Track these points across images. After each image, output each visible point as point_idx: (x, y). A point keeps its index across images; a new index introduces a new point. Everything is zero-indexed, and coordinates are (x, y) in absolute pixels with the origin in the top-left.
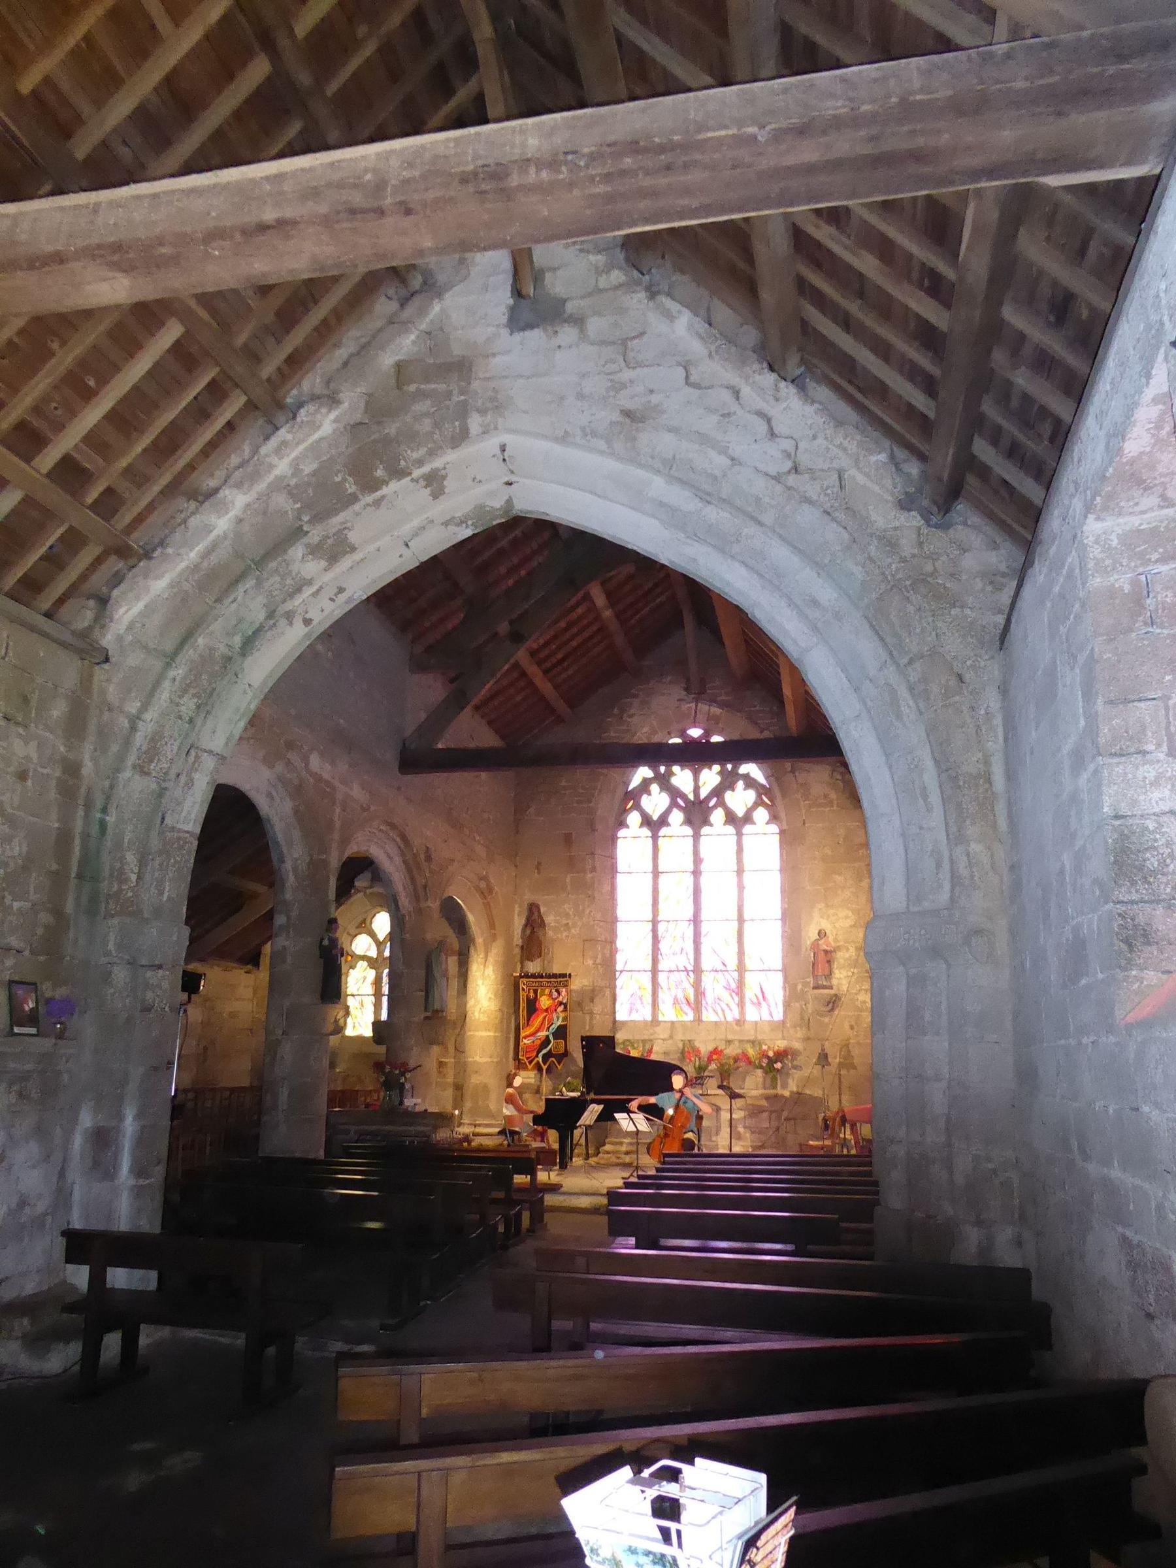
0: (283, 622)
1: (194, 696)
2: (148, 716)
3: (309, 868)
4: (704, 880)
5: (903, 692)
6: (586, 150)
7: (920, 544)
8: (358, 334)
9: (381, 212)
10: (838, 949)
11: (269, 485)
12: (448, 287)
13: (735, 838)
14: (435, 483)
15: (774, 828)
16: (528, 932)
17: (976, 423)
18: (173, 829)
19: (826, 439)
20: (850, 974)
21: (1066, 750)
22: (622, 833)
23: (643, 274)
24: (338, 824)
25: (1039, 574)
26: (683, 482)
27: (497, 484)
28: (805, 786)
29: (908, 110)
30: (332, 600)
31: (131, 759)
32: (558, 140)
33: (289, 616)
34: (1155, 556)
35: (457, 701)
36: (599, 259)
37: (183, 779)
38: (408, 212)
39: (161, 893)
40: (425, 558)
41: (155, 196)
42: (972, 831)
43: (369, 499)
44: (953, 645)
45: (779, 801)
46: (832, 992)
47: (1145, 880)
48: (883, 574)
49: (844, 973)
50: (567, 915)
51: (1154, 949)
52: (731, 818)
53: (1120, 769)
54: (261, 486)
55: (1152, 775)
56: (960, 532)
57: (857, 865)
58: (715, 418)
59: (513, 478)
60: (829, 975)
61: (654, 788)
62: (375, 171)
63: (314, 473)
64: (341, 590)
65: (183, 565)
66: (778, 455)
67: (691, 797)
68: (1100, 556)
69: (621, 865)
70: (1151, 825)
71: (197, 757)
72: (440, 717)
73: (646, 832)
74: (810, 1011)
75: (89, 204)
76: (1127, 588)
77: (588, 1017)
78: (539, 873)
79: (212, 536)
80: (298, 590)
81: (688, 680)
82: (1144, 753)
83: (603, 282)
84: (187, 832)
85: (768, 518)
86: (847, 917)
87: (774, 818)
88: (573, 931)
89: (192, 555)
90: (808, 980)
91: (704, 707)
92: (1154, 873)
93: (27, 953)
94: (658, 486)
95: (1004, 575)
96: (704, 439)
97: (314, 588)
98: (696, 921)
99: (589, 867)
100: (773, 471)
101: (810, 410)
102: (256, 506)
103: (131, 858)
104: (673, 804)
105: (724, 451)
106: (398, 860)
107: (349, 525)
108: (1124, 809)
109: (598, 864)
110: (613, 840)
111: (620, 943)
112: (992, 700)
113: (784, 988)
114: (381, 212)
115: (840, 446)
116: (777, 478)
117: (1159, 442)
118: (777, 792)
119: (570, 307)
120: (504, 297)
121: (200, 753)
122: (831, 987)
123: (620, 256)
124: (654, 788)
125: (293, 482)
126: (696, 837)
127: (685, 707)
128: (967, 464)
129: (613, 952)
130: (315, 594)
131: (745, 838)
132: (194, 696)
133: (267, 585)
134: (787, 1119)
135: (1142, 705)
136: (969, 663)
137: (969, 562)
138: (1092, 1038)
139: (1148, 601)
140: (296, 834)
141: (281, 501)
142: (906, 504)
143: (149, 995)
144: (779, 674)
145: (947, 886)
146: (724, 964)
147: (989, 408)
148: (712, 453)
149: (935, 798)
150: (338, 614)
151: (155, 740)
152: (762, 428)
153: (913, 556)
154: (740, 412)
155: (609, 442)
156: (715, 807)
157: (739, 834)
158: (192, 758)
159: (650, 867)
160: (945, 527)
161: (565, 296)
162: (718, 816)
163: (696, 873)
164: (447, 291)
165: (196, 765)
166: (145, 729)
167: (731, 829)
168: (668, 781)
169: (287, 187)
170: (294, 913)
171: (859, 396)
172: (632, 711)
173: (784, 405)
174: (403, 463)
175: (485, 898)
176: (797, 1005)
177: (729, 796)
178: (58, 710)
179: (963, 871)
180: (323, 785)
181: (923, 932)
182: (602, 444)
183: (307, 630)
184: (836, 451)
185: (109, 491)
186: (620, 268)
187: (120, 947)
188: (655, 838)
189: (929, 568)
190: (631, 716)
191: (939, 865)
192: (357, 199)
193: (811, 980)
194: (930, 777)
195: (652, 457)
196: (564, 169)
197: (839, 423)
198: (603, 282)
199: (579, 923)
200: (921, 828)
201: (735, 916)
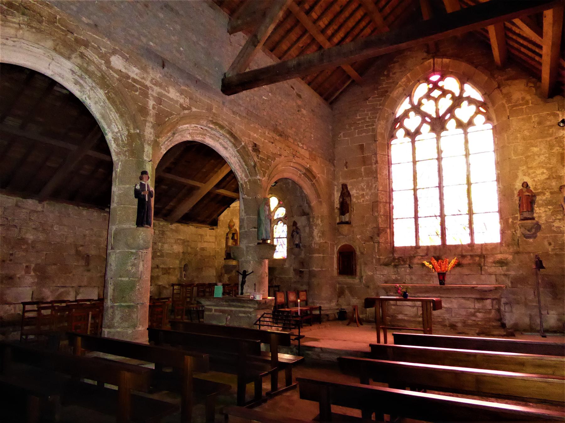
3: (128, 139)
4: (443, 163)
10: (539, 194)
13: (463, 135)
15: (489, 126)
16: (341, 200)
22: (393, 142)
24: (152, 112)
28: (508, 97)
35: (253, 42)
45: (491, 110)
49: (543, 209)
50: (363, 190)
52: (460, 124)
57: (548, 139)
60: (532, 210)
61: (412, 114)
67: (434, 115)
69: (394, 160)
73: (408, 139)
74: (519, 235)
77: (376, 245)
78: (347, 168)
86: (543, 173)
87: (489, 119)
88: (366, 197)
90: (516, 215)
98: (440, 187)
104: (424, 121)
109: (379, 159)
110: (389, 146)
111: (395, 203)
113: (500, 222)
118: (490, 105)
122: (533, 219)
124: (412, 114)
126: (438, 138)
127: (426, 63)
129: (391, 209)
131: (469, 135)
134: (506, 304)
146: (459, 211)
156: (450, 118)
157: (466, 133)
162: (451, 124)
163: (439, 159)
167: (461, 131)
168: (419, 109)
172: (395, 71)
175: (312, 181)
176: (509, 232)
180: (130, 81)
188: (413, 142)
190: (394, 73)
193: (518, 215)
199: (370, 193)
201: (465, 182)
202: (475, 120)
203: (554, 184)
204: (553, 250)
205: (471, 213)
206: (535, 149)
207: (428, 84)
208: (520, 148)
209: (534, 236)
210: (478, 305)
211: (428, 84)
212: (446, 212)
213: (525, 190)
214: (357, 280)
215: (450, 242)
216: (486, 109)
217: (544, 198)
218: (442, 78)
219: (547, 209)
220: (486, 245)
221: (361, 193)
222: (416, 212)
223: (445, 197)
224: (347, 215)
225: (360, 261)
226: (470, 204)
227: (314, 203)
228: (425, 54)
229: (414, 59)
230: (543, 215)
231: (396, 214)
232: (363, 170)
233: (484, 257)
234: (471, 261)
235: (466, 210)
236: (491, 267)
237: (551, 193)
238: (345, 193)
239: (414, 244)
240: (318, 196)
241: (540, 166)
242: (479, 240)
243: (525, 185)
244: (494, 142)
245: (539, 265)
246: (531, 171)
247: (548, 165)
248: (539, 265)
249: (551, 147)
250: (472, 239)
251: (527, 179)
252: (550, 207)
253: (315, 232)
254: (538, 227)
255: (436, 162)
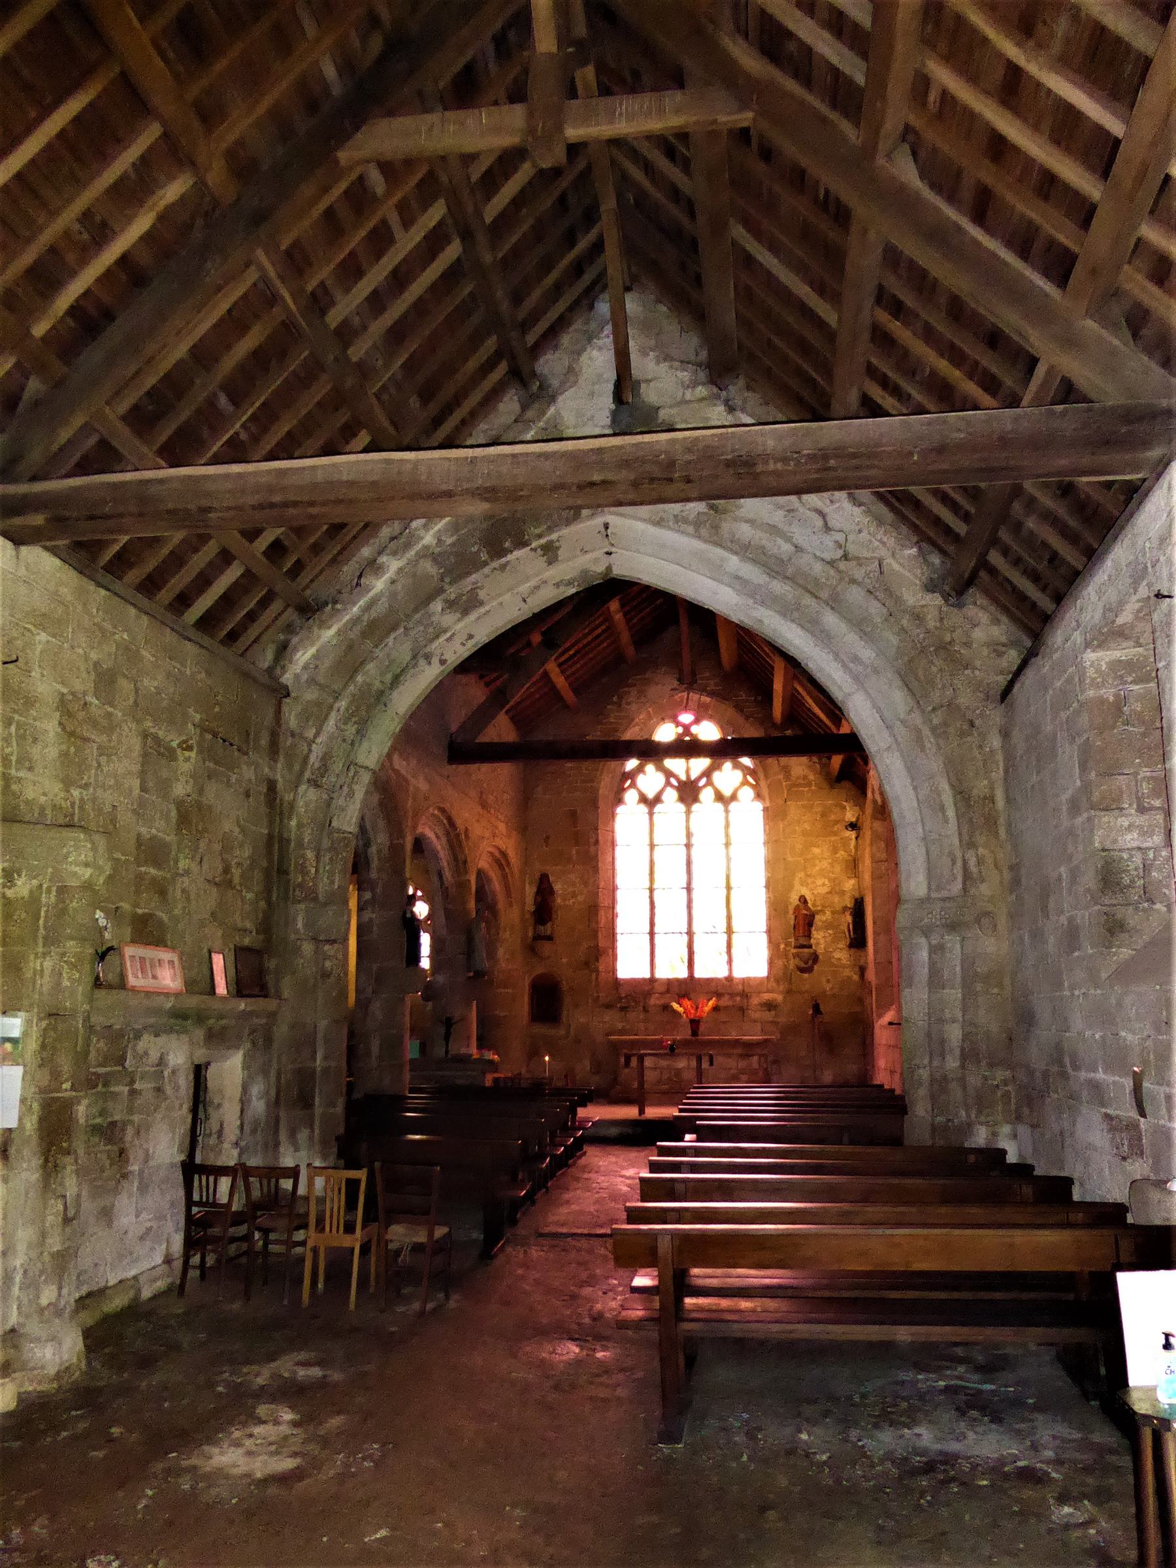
0: (422, 662)
1: (355, 723)
2: (319, 740)
4: (694, 851)
5: (926, 732)
6: (805, 452)
7: (942, 619)
8: (486, 427)
9: (671, 480)
10: (818, 912)
11: (417, 553)
12: (562, 389)
14: (550, 552)
17: (994, 541)
18: (339, 831)
19: (870, 534)
20: (827, 935)
21: (1065, 797)
23: (721, 390)
25: (1042, 666)
26: (754, 561)
27: (599, 553)
29: (1004, 441)
30: (463, 645)
31: (307, 775)
32: (787, 443)
33: (428, 658)
34: (1130, 679)
35: (498, 699)
36: (685, 376)
37: (345, 789)
38: (689, 481)
39: (333, 882)
40: (536, 610)
41: (514, 456)
42: (980, 839)
43: (496, 564)
44: (965, 699)
45: (763, 783)
46: (811, 951)
47: (1121, 891)
48: (913, 641)
49: (822, 934)
50: (574, 885)
51: (1126, 935)
52: (719, 797)
53: (1106, 819)
54: (412, 553)
55: (1126, 824)
56: (971, 611)
57: (833, 839)
58: (781, 513)
59: (613, 550)
60: (809, 936)
62: (666, 452)
63: (453, 545)
64: (471, 637)
65: (348, 617)
66: (831, 545)
68: (1093, 676)
70: (1125, 856)
71: (356, 773)
72: (483, 715)
73: (643, 808)
75: (467, 458)
76: (1111, 699)
79: (371, 594)
80: (437, 637)
81: (681, 671)
82: (1121, 809)
83: (689, 395)
84: (350, 833)
85: (824, 594)
87: (759, 796)
88: (579, 898)
89: (355, 609)
91: (694, 696)
92: (1129, 886)
93: (254, 933)
94: (733, 562)
95: (1004, 645)
96: (773, 530)
97: (448, 635)
99: (592, 840)
100: (828, 556)
101: (857, 511)
102: (407, 570)
103: (310, 855)
104: (668, 783)
105: (789, 539)
106: (444, 840)
107: (479, 584)
108: (1108, 845)
110: (613, 815)
112: (996, 742)
113: (769, 947)
114: (671, 480)
115: (881, 541)
116: (831, 563)
117: (1137, 618)
118: (761, 775)
119: (663, 414)
120: (606, 402)
121: (358, 768)
122: (810, 947)
123: (702, 375)
125: (437, 550)
126: (688, 812)
128: (984, 564)
130: (448, 640)
132: (355, 723)
133: (412, 633)
135: (1120, 777)
136: (978, 712)
137: (978, 634)
138: (1083, 990)
139: (1125, 708)
140: (381, 823)
141: (428, 567)
142: (931, 587)
143: (328, 964)
144: (773, 675)
145: (960, 879)
147: (1004, 535)
148: (780, 541)
149: (951, 813)
150: (466, 654)
151: (326, 759)
152: (819, 523)
153: (936, 628)
154: (801, 510)
155: (697, 529)
156: (705, 786)
158: (351, 774)
159: (648, 842)
160: (960, 606)
161: (658, 405)
162: (707, 795)
163: (688, 846)
164: (561, 394)
165: (356, 779)
166: (317, 751)
167: (720, 806)
169: (606, 457)
170: (379, 890)
171: (897, 504)
172: (631, 699)
173: (837, 505)
174: (526, 537)
177: (717, 776)
178: (264, 741)
179: (974, 869)
181: (943, 913)
182: (691, 529)
183: (442, 668)
184: (877, 543)
185: (298, 561)
186: (703, 384)
187: (306, 925)
188: (651, 814)
189: (948, 638)
190: (628, 704)
191: (954, 862)
192: (656, 471)
193: (792, 940)
194: (948, 798)
195: (732, 542)
196: (792, 463)
197: (880, 522)
198: (689, 395)
200: (940, 835)
202: (740, 794)
203: (836, 900)
204: (832, 989)
205: (729, 931)
206: (816, 851)
207: (677, 726)
208: (799, 847)
209: (809, 970)
210: (742, 1064)
211: (677, 726)
212: (695, 928)
213: (802, 906)
214: (562, 1032)
215: (699, 973)
216: (755, 780)
217: (824, 918)
218: (697, 721)
219: (827, 935)
220: (749, 979)
221: (571, 889)
222: (652, 924)
223: (695, 905)
224: (549, 925)
225: (567, 1000)
226: (729, 918)
227: (501, 905)
228: (676, 683)
229: (660, 686)
230: (822, 941)
231: (621, 925)
232: (574, 852)
233: (747, 996)
234: (730, 1003)
235: (723, 927)
236: (756, 1012)
237: (833, 913)
238: (544, 890)
239: (648, 976)
240: (508, 894)
241: (822, 873)
242: (739, 973)
243: (802, 901)
244: (765, 830)
245: (817, 1009)
246: (809, 881)
247: (831, 875)
248: (817, 1009)
249: (835, 850)
250: (730, 970)
251: (805, 892)
252: (830, 932)
253: (501, 952)
254: (815, 958)
255: (684, 849)
